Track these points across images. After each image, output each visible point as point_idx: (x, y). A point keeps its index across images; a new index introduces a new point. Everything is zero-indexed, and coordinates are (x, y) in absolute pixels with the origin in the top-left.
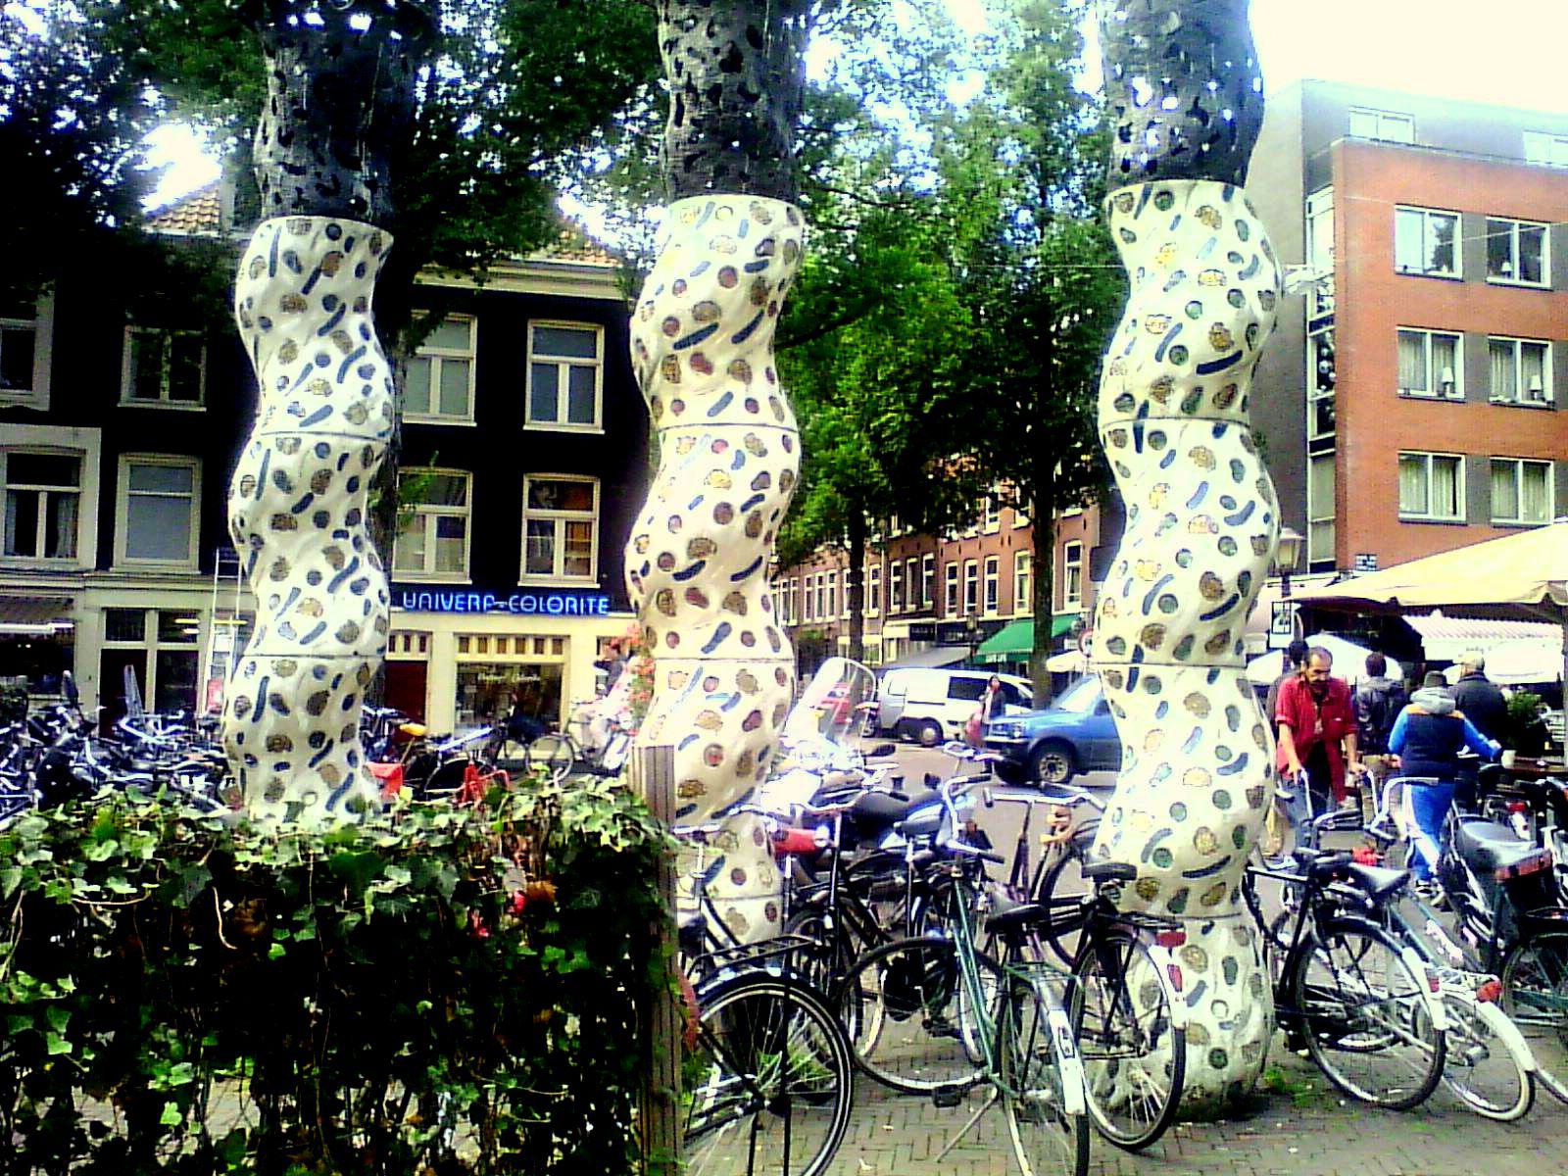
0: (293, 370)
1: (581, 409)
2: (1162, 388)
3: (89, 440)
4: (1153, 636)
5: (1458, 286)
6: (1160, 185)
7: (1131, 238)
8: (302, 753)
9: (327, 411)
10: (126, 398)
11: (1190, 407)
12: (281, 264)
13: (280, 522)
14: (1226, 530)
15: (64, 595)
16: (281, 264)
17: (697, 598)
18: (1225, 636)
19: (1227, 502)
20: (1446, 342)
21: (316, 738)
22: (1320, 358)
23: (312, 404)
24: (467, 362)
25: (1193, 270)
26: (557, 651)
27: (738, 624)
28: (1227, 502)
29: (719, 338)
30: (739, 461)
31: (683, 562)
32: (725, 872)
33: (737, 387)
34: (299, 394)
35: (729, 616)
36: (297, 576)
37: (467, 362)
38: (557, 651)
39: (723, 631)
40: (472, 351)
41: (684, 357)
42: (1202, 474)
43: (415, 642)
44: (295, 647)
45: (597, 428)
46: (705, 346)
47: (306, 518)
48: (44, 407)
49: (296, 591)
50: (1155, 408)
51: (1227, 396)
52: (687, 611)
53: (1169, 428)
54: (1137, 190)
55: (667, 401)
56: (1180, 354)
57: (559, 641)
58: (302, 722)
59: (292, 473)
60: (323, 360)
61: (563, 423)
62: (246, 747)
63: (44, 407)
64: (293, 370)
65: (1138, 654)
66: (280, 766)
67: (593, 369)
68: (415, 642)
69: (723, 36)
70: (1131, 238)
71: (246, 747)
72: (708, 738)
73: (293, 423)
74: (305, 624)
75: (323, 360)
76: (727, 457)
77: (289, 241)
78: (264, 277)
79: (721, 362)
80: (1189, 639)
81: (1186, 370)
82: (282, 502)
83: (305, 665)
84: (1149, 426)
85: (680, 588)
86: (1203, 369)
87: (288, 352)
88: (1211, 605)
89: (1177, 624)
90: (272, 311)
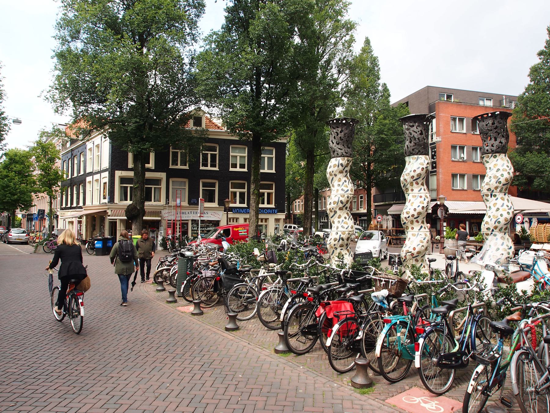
0: (341, 183)
1: (270, 168)
2: (496, 188)
3: (163, 175)
4: (496, 228)
5: (464, 135)
6: (494, 155)
7: (488, 162)
8: (345, 247)
9: (348, 190)
10: (171, 167)
11: (501, 191)
12: (340, 166)
13: (341, 209)
14: (508, 211)
15: (159, 210)
16: (340, 166)
17: (417, 222)
18: (507, 227)
19: (508, 206)
20: (462, 148)
21: (347, 245)
22: (432, 152)
23: (346, 189)
24: (245, 157)
25: (501, 168)
26: (266, 222)
27: (423, 226)
28: (508, 206)
29: (421, 179)
30: (425, 200)
31: (416, 216)
32: (422, 266)
33: (422, 187)
34: (343, 187)
35: (422, 225)
36: (343, 218)
37: (245, 157)
38: (266, 222)
39: (421, 227)
40: (246, 155)
41: (414, 183)
42: (502, 202)
43: (235, 220)
44: (345, 230)
45: (273, 171)
46: (418, 181)
47: (344, 208)
48: (153, 168)
49: (343, 221)
50: (495, 191)
51: (506, 190)
52: (415, 223)
53: (497, 194)
54: (490, 155)
55: (410, 189)
56: (500, 182)
57: (266, 220)
58: (346, 242)
59: (343, 201)
60: (345, 181)
61: (266, 170)
62: (336, 246)
63: (153, 168)
64: (341, 183)
65: (493, 231)
66: (341, 249)
67: (272, 158)
68: (235, 220)
69: (419, 129)
70: (488, 162)
71: (336, 246)
72: (422, 244)
73: (343, 192)
74: (346, 226)
75: (345, 181)
76: (423, 199)
77: (341, 162)
78: (337, 168)
79: (420, 183)
80: (502, 228)
81: (501, 185)
82: (341, 205)
83: (347, 233)
84: (493, 194)
85: (415, 220)
86: (504, 185)
87: (340, 180)
88: (506, 223)
89: (500, 226)
90: (337, 173)
